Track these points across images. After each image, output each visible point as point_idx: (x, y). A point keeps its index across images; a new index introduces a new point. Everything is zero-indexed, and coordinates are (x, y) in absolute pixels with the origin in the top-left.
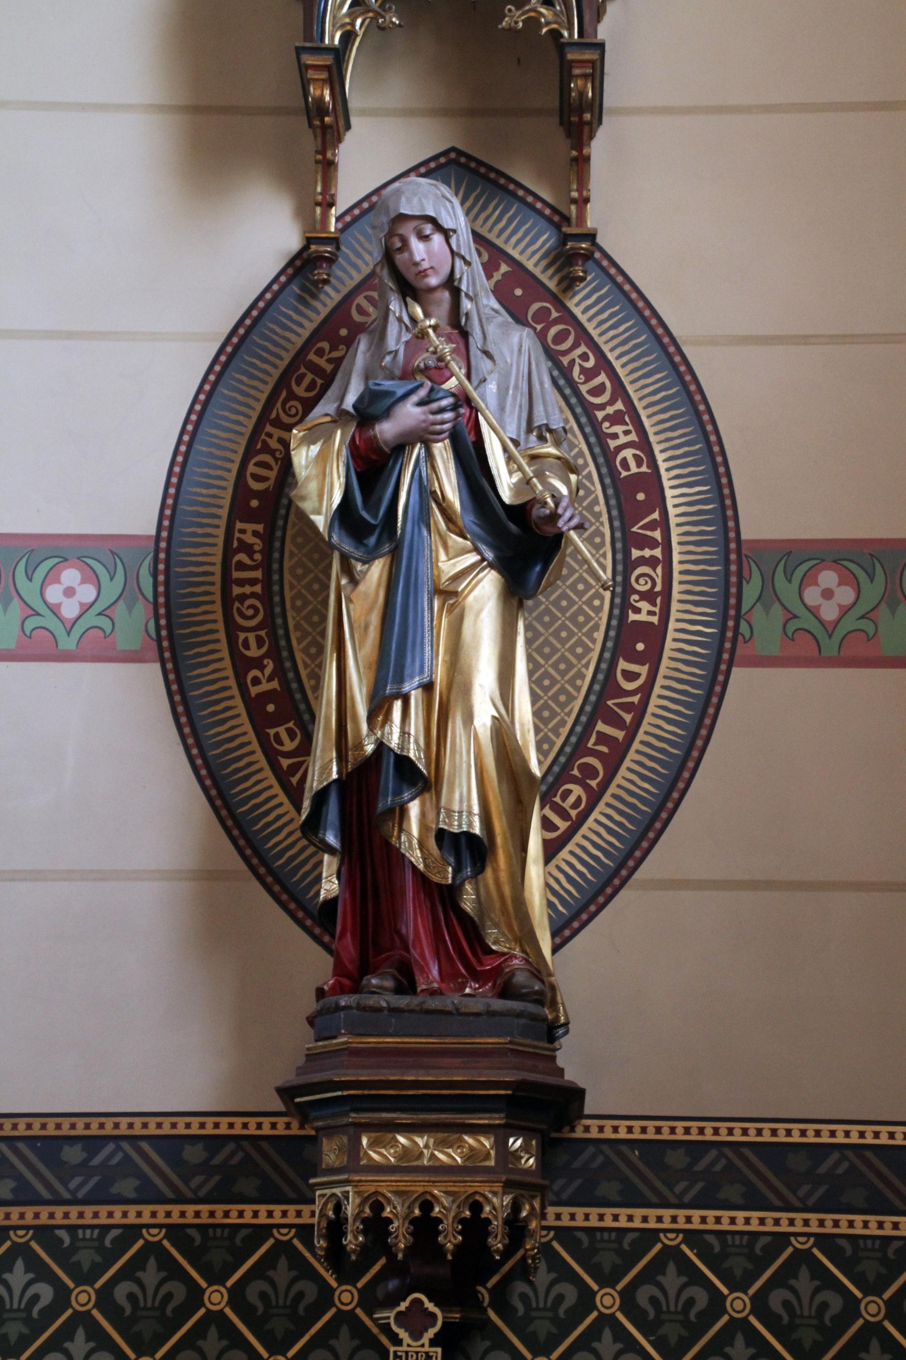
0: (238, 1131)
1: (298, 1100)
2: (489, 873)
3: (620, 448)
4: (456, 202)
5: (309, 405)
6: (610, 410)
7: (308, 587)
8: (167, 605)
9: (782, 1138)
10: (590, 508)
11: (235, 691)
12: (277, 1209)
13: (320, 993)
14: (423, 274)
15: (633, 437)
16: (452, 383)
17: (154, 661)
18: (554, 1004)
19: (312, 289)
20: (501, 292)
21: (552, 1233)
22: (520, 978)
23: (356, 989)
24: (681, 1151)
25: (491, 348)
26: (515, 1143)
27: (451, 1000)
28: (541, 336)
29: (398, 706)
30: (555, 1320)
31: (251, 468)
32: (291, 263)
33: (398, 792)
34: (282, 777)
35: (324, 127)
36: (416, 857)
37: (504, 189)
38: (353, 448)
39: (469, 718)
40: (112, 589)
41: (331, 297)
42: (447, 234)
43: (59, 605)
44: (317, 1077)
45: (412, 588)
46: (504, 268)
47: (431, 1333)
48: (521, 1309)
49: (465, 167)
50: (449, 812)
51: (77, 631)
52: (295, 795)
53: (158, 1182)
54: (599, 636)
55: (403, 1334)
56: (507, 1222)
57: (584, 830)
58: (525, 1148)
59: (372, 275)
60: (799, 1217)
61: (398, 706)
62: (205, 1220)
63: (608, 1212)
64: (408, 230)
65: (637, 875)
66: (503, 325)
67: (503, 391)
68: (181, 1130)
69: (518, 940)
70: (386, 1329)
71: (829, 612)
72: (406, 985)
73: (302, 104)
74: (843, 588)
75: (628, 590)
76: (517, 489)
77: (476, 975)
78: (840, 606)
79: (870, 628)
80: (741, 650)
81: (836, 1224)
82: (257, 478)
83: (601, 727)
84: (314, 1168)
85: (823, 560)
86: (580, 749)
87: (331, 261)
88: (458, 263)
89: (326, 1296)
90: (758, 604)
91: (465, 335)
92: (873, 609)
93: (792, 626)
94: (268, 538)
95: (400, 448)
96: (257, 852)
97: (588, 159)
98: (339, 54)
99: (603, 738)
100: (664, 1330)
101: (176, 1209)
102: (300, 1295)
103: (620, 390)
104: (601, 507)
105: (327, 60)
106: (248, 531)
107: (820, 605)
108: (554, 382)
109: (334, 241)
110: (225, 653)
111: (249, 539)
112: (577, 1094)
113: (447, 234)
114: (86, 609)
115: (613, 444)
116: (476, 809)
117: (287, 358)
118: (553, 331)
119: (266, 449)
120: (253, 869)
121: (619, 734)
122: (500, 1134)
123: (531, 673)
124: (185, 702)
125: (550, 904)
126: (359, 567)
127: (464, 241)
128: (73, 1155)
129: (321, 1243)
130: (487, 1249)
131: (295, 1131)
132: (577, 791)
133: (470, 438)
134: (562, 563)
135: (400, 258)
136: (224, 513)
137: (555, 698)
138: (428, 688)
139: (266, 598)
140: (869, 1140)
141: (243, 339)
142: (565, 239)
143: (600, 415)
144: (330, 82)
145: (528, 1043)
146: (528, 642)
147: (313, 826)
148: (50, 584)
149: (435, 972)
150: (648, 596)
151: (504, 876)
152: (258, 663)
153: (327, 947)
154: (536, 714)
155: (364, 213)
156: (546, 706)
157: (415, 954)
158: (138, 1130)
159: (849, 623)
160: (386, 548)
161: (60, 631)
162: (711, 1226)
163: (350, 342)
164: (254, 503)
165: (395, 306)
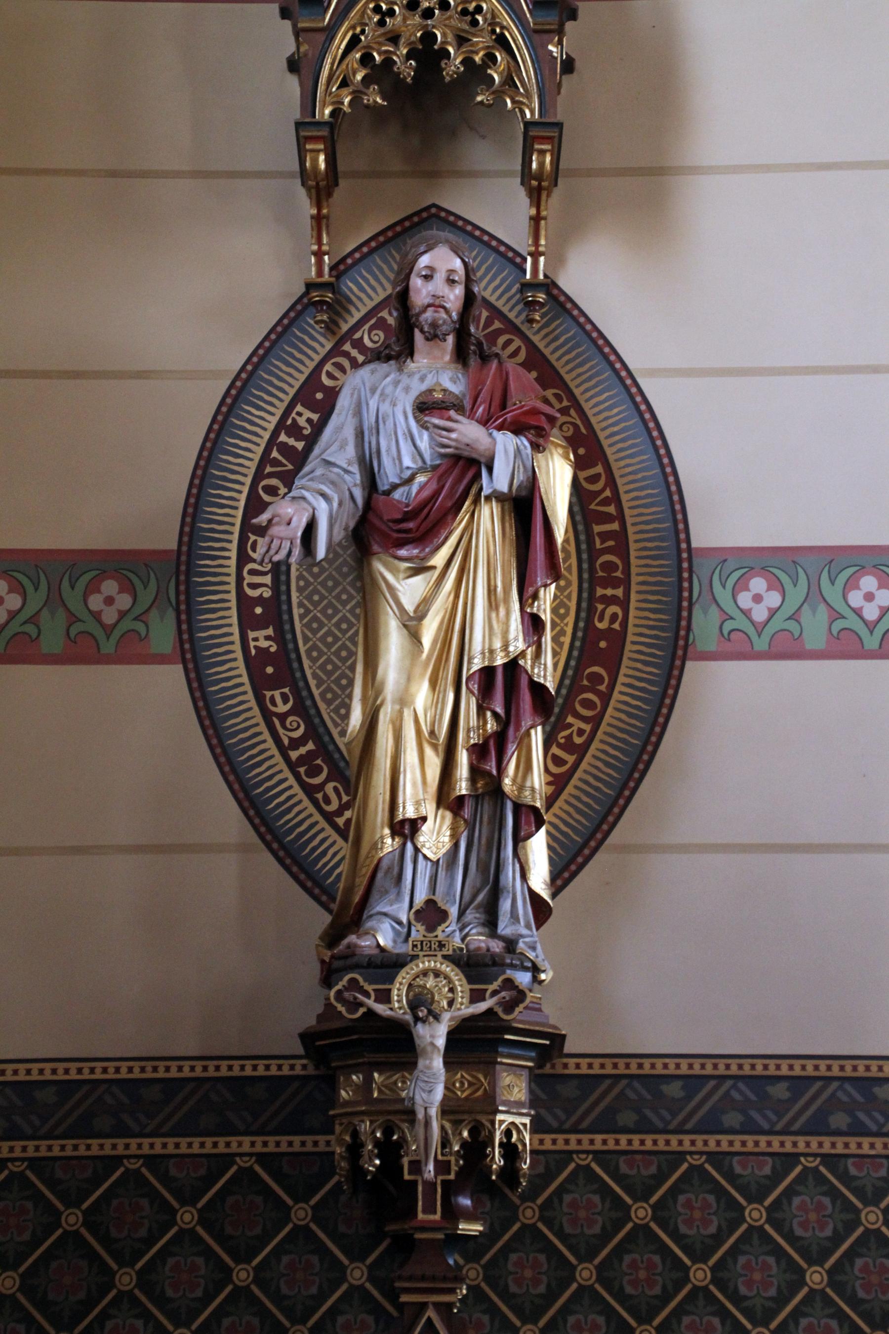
1: (318, 1043)
17: (723, 555)
21: (704, 1157)
24: (784, 1085)
51: (117, 634)
71: (760, 614)
73: (296, 167)
74: (13, 595)
79: (31, 629)
81: (316, 1144)
85: (752, 568)
90: (45, 608)
92: (144, 613)
96: (270, 830)
148: (850, 591)
161: (863, 632)
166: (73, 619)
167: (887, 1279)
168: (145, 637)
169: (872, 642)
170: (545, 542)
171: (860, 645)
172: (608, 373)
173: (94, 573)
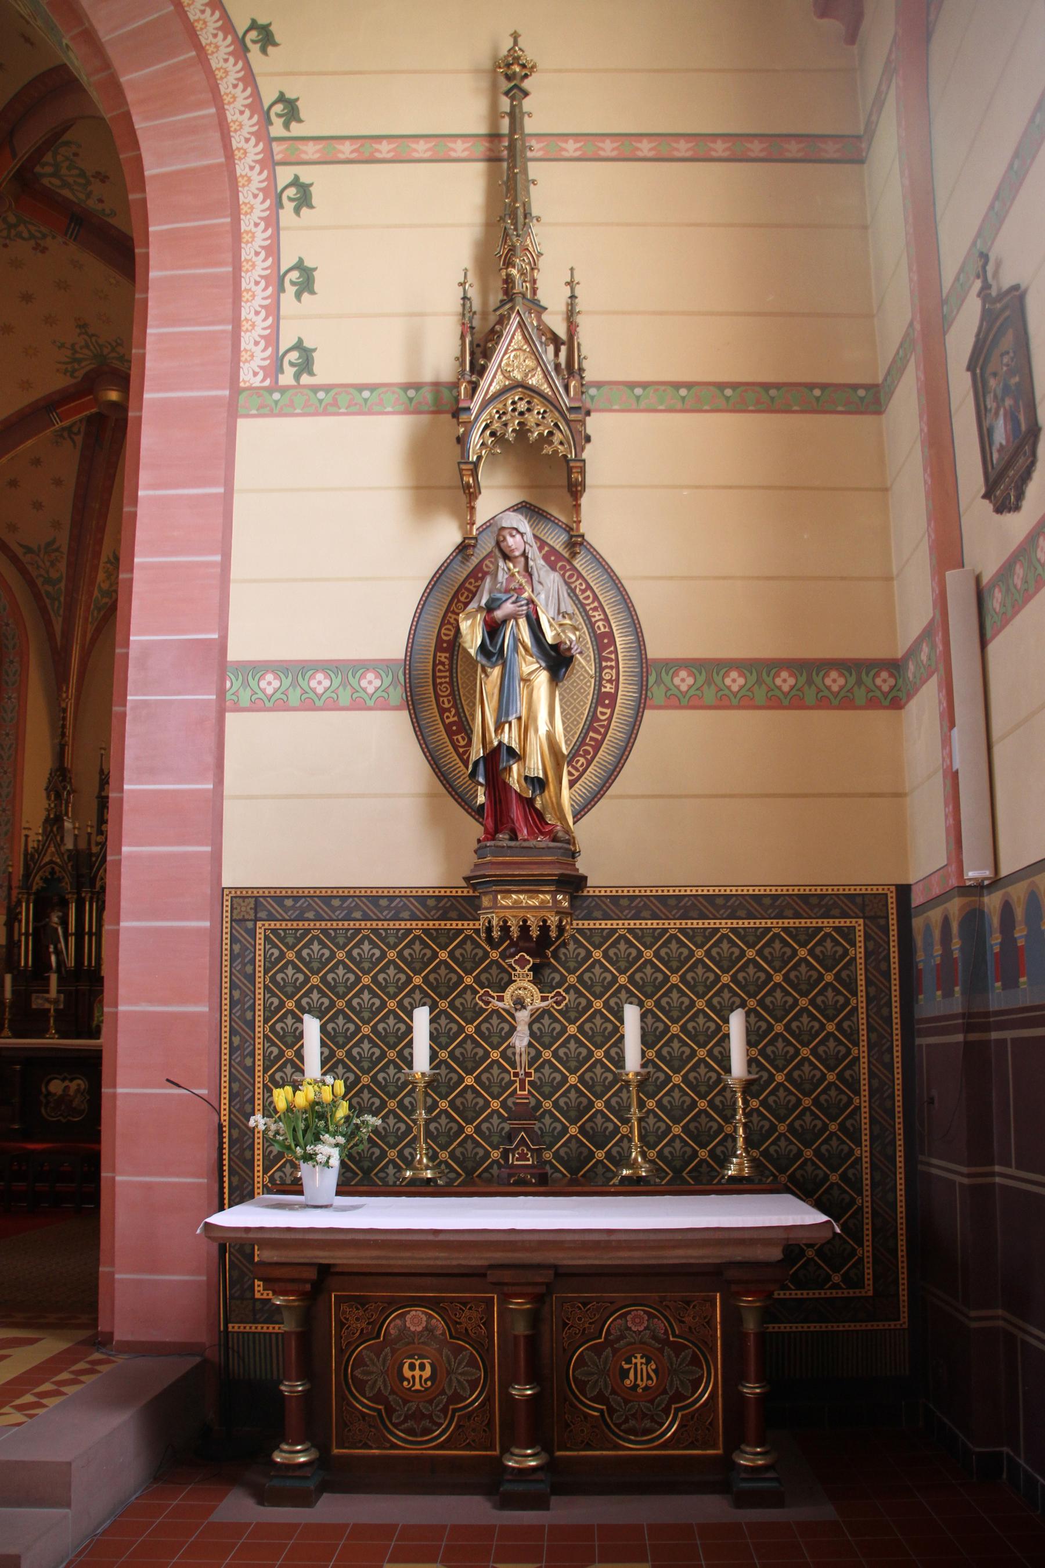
0: (448, 894)
2: (546, 792)
3: (596, 622)
4: (526, 522)
5: (466, 605)
6: (592, 606)
7: (468, 679)
8: (410, 687)
9: (666, 893)
10: (585, 645)
11: (439, 721)
12: (466, 923)
13: (479, 841)
14: (512, 551)
15: (602, 617)
16: (526, 595)
18: (574, 844)
19: (467, 558)
20: (545, 558)
22: (560, 834)
23: (493, 839)
25: (542, 580)
26: (560, 897)
27: (532, 843)
28: (563, 576)
29: (507, 726)
30: (577, 962)
31: (443, 631)
32: (457, 548)
33: (508, 761)
34: (460, 756)
35: (470, 494)
36: (516, 787)
37: (546, 517)
38: (485, 621)
39: (536, 731)
40: (387, 681)
41: (475, 561)
42: (522, 534)
44: (478, 873)
45: (511, 678)
46: (546, 549)
47: (528, 967)
48: (563, 958)
49: (529, 508)
50: (529, 769)
52: (466, 764)
53: (418, 913)
54: (590, 697)
55: (517, 967)
56: (557, 926)
57: (585, 776)
58: (564, 899)
59: (491, 552)
60: (672, 922)
61: (507, 726)
62: (437, 927)
63: (598, 922)
64: (506, 533)
65: (608, 793)
66: (547, 571)
67: (547, 598)
68: (425, 894)
69: (559, 819)
70: (510, 966)
72: (514, 837)
75: (601, 679)
76: (554, 637)
77: (542, 833)
80: (648, 702)
82: (445, 635)
83: (591, 734)
84: (479, 908)
86: (583, 743)
87: (474, 546)
88: (527, 547)
89: (486, 955)
91: (531, 575)
93: (669, 694)
94: (451, 659)
95: (505, 621)
97: (580, 505)
98: (476, 464)
99: (592, 739)
100: (620, 964)
101: (425, 923)
102: (476, 954)
103: (596, 598)
104: (589, 645)
105: (471, 467)
106: (443, 657)
108: (569, 595)
109: (476, 538)
110: (435, 706)
111: (443, 659)
112: (584, 879)
113: (522, 534)
114: (377, 689)
115: (594, 620)
116: (540, 767)
117: (457, 586)
118: (567, 574)
119: (449, 623)
120: (450, 793)
121: (599, 737)
122: (554, 894)
123: (562, 713)
124: (419, 726)
125: (572, 805)
126: (489, 670)
127: (529, 537)
128: (384, 903)
129: (483, 935)
130: (549, 936)
131: (471, 894)
132: (582, 760)
133: (534, 617)
134: (573, 668)
135: (503, 545)
136: (433, 649)
137: (572, 723)
138: (519, 719)
139: (451, 683)
140: (700, 893)
141: (438, 579)
142: (572, 537)
143: (588, 608)
144: (472, 475)
145: (564, 859)
146: (561, 700)
147: (473, 775)
149: (525, 832)
150: (610, 681)
151: (553, 794)
152: (448, 710)
153: (481, 823)
154: (565, 729)
155: (488, 527)
156: (568, 713)
157: (517, 825)
158: (408, 894)
159: (692, 692)
160: (500, 662)
161: (831, 697)
162: (638, 926)
163: (483, 579)
164: (445, 645)
165: (501, 563)
166: (819, 691)
169: (786, 702)
172: (443, 577)
173: (311, 672)
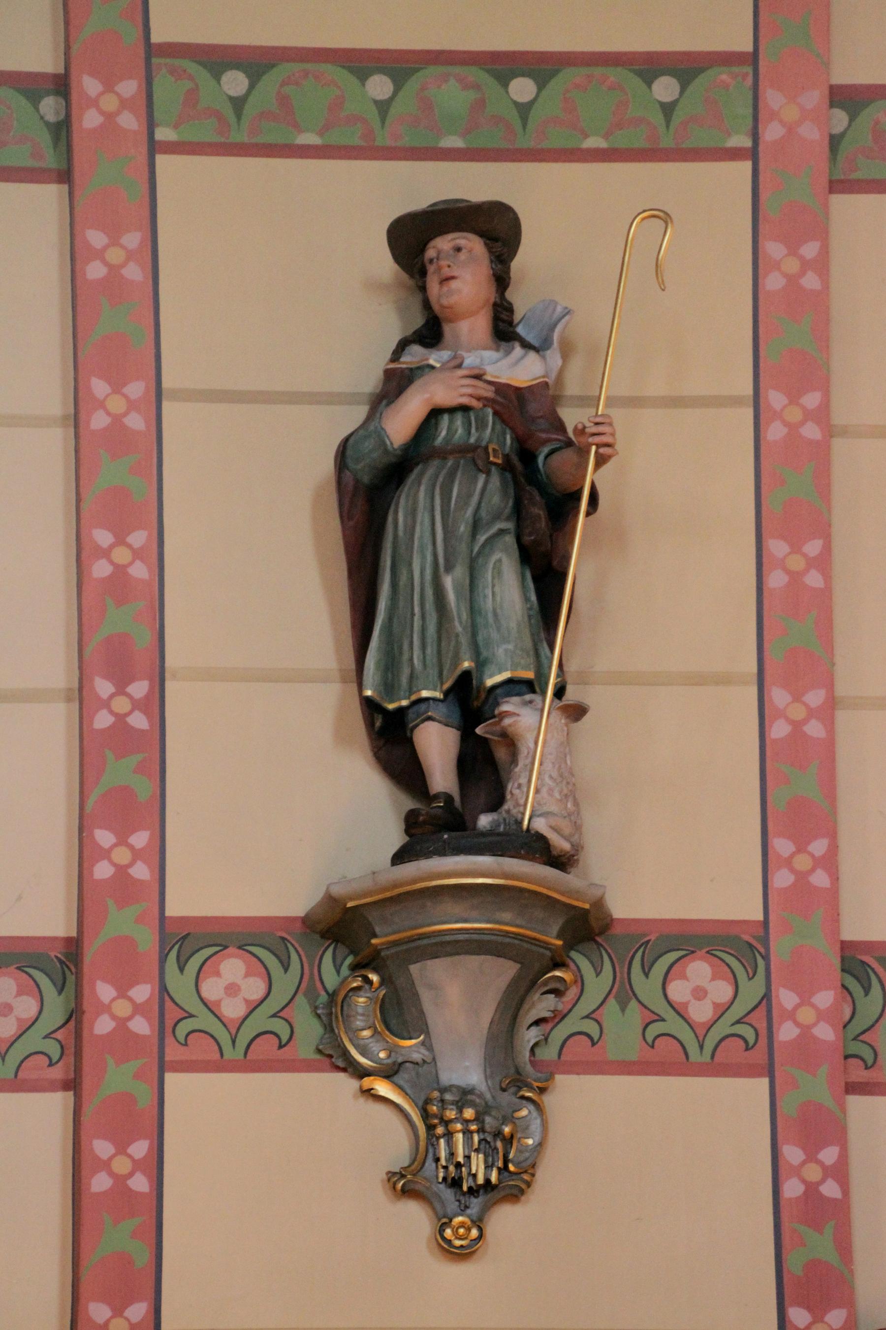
43: (716, 1005)
74: (251, 980)
78: (246, 1001)
79: (591, 1027)
107: (714, 1003)
159: (260, 1021)
167: (5, 1009)
168: (753, 1047)
170: (499, 683)
171: (684, 1057)
